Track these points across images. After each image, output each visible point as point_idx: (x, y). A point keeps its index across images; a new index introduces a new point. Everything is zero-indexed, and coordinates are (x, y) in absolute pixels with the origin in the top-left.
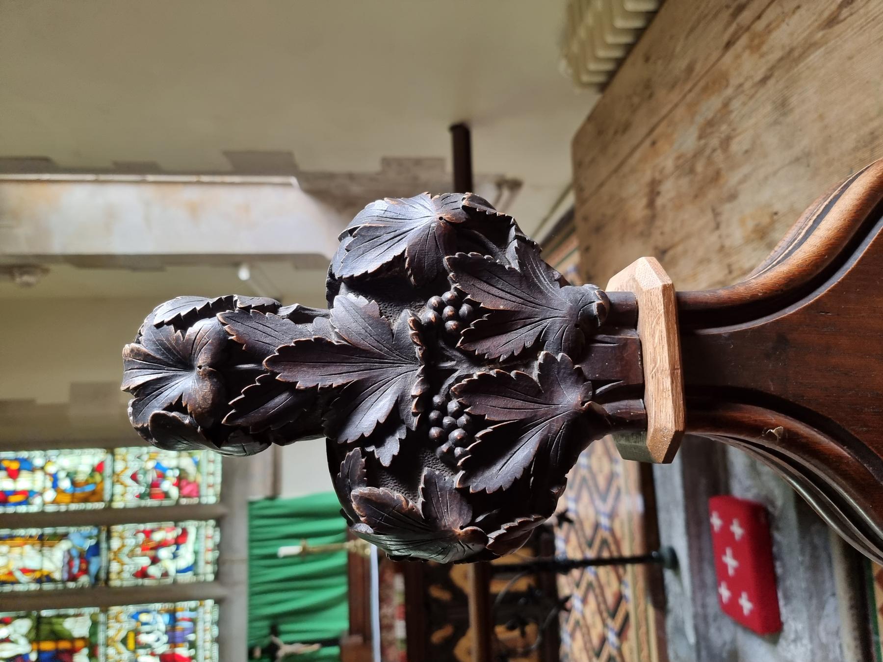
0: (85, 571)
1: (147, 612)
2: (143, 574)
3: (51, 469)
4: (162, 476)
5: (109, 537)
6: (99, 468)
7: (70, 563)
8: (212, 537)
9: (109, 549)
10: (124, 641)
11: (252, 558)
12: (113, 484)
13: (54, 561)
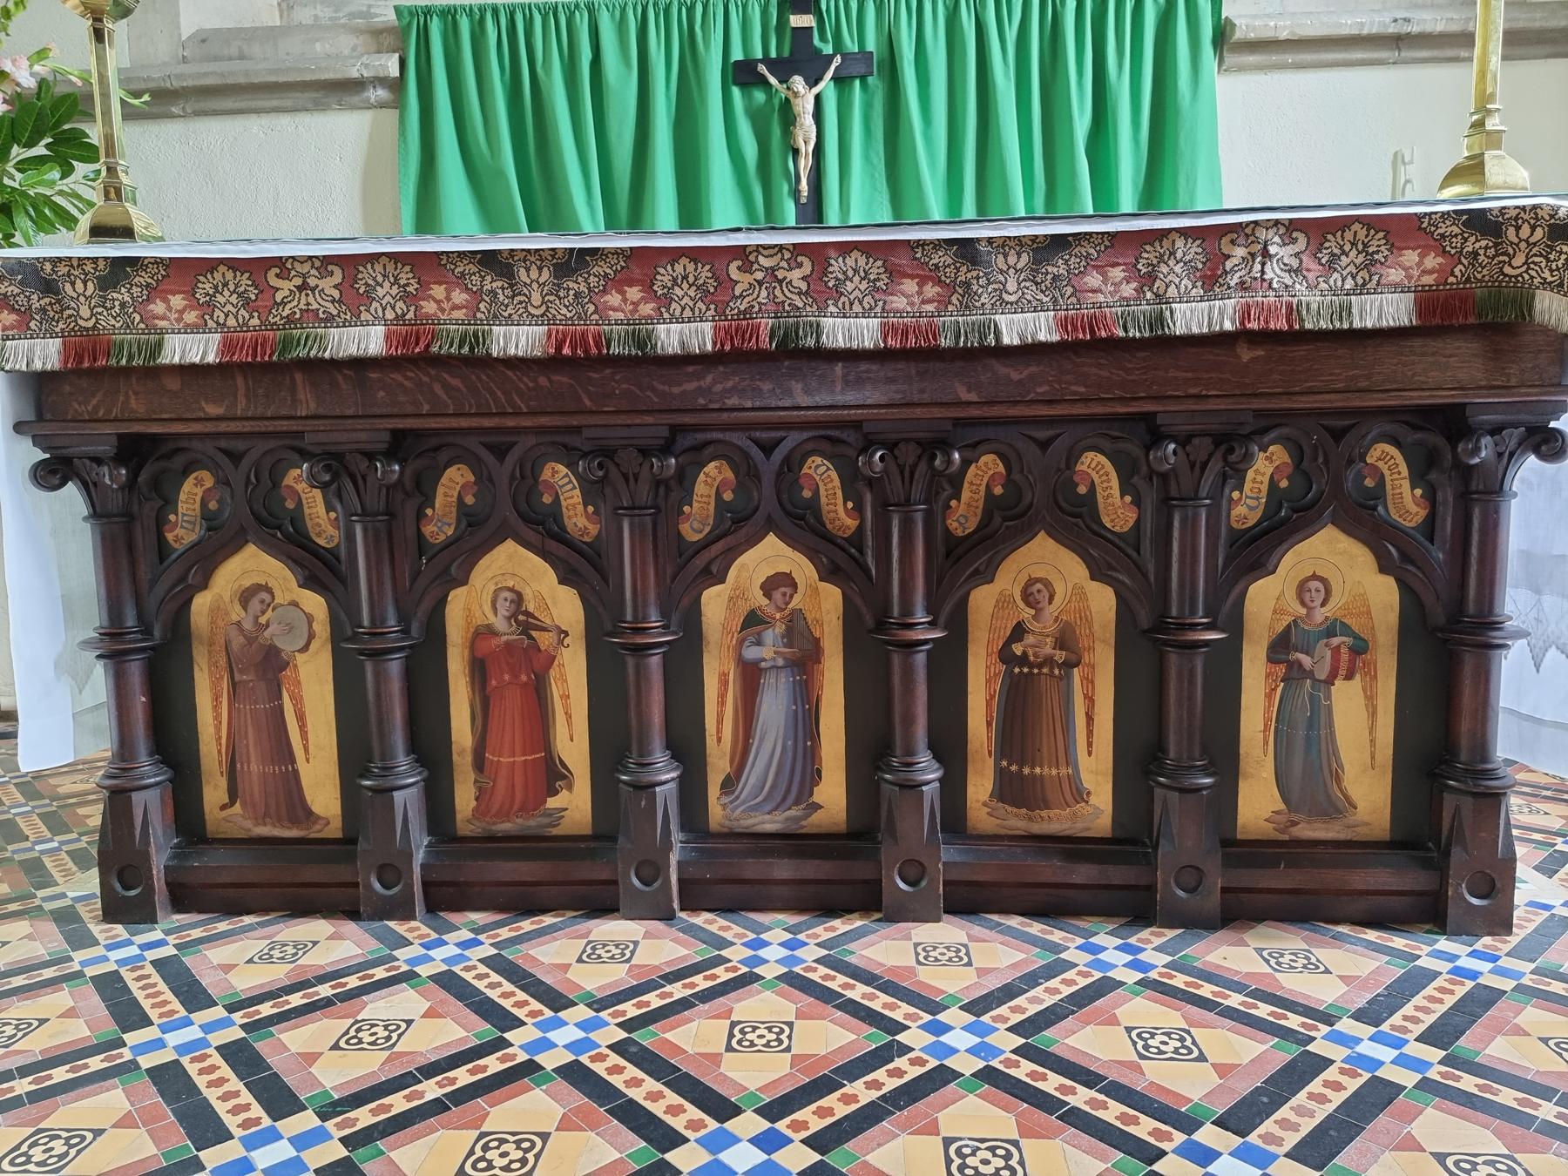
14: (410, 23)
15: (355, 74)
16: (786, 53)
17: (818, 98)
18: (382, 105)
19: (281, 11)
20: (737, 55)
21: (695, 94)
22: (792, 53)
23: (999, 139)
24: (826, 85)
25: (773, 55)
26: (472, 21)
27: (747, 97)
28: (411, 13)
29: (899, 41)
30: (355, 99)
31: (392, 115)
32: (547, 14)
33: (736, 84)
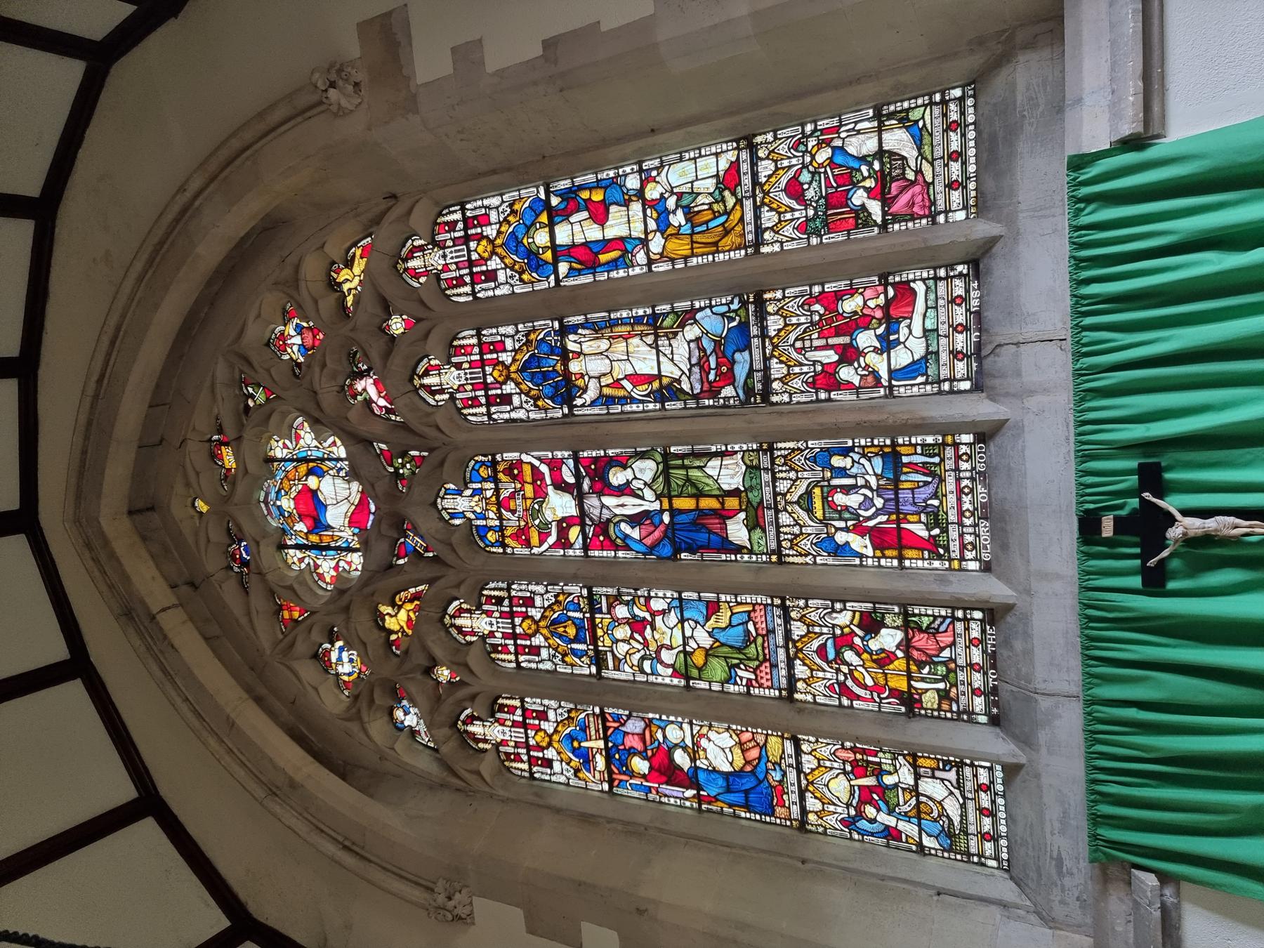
0: (729, 379)
1: (845, 452)
2: (827, 379)
3: (652, 192)
4: (849, 179)
5: (762, 316)
6: (729, 180)
7: (702, 364)
8: (964, 300)
9: (764, 335)
10: (806, 501)
11: (1082, 307)
12: (757, 209)
13: (676, 360)
14: (1105, 853)
15: (1158, 914)
16: (1137, 539)
17: (1186, 513)
18: (1178, 894)
19: (1056, 928)
20: (1136, 582)
21: (1163, 622)
22: (1136, 535)
23: (1233, 340)
24: (1170, 504)
25: (1138, 550)
26: (1102, 802)
27: (1174, 575)
28: (1095, 851)
29: (1129, 441)
30: (1174, 914)
31: (1185, 886)
32: (1095, 739)
33: (1163, 586)
